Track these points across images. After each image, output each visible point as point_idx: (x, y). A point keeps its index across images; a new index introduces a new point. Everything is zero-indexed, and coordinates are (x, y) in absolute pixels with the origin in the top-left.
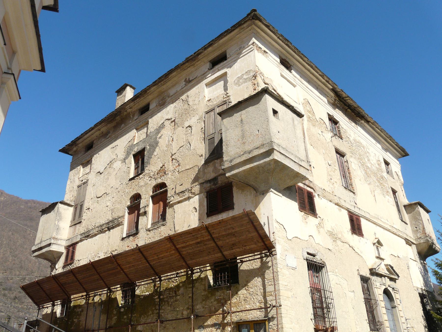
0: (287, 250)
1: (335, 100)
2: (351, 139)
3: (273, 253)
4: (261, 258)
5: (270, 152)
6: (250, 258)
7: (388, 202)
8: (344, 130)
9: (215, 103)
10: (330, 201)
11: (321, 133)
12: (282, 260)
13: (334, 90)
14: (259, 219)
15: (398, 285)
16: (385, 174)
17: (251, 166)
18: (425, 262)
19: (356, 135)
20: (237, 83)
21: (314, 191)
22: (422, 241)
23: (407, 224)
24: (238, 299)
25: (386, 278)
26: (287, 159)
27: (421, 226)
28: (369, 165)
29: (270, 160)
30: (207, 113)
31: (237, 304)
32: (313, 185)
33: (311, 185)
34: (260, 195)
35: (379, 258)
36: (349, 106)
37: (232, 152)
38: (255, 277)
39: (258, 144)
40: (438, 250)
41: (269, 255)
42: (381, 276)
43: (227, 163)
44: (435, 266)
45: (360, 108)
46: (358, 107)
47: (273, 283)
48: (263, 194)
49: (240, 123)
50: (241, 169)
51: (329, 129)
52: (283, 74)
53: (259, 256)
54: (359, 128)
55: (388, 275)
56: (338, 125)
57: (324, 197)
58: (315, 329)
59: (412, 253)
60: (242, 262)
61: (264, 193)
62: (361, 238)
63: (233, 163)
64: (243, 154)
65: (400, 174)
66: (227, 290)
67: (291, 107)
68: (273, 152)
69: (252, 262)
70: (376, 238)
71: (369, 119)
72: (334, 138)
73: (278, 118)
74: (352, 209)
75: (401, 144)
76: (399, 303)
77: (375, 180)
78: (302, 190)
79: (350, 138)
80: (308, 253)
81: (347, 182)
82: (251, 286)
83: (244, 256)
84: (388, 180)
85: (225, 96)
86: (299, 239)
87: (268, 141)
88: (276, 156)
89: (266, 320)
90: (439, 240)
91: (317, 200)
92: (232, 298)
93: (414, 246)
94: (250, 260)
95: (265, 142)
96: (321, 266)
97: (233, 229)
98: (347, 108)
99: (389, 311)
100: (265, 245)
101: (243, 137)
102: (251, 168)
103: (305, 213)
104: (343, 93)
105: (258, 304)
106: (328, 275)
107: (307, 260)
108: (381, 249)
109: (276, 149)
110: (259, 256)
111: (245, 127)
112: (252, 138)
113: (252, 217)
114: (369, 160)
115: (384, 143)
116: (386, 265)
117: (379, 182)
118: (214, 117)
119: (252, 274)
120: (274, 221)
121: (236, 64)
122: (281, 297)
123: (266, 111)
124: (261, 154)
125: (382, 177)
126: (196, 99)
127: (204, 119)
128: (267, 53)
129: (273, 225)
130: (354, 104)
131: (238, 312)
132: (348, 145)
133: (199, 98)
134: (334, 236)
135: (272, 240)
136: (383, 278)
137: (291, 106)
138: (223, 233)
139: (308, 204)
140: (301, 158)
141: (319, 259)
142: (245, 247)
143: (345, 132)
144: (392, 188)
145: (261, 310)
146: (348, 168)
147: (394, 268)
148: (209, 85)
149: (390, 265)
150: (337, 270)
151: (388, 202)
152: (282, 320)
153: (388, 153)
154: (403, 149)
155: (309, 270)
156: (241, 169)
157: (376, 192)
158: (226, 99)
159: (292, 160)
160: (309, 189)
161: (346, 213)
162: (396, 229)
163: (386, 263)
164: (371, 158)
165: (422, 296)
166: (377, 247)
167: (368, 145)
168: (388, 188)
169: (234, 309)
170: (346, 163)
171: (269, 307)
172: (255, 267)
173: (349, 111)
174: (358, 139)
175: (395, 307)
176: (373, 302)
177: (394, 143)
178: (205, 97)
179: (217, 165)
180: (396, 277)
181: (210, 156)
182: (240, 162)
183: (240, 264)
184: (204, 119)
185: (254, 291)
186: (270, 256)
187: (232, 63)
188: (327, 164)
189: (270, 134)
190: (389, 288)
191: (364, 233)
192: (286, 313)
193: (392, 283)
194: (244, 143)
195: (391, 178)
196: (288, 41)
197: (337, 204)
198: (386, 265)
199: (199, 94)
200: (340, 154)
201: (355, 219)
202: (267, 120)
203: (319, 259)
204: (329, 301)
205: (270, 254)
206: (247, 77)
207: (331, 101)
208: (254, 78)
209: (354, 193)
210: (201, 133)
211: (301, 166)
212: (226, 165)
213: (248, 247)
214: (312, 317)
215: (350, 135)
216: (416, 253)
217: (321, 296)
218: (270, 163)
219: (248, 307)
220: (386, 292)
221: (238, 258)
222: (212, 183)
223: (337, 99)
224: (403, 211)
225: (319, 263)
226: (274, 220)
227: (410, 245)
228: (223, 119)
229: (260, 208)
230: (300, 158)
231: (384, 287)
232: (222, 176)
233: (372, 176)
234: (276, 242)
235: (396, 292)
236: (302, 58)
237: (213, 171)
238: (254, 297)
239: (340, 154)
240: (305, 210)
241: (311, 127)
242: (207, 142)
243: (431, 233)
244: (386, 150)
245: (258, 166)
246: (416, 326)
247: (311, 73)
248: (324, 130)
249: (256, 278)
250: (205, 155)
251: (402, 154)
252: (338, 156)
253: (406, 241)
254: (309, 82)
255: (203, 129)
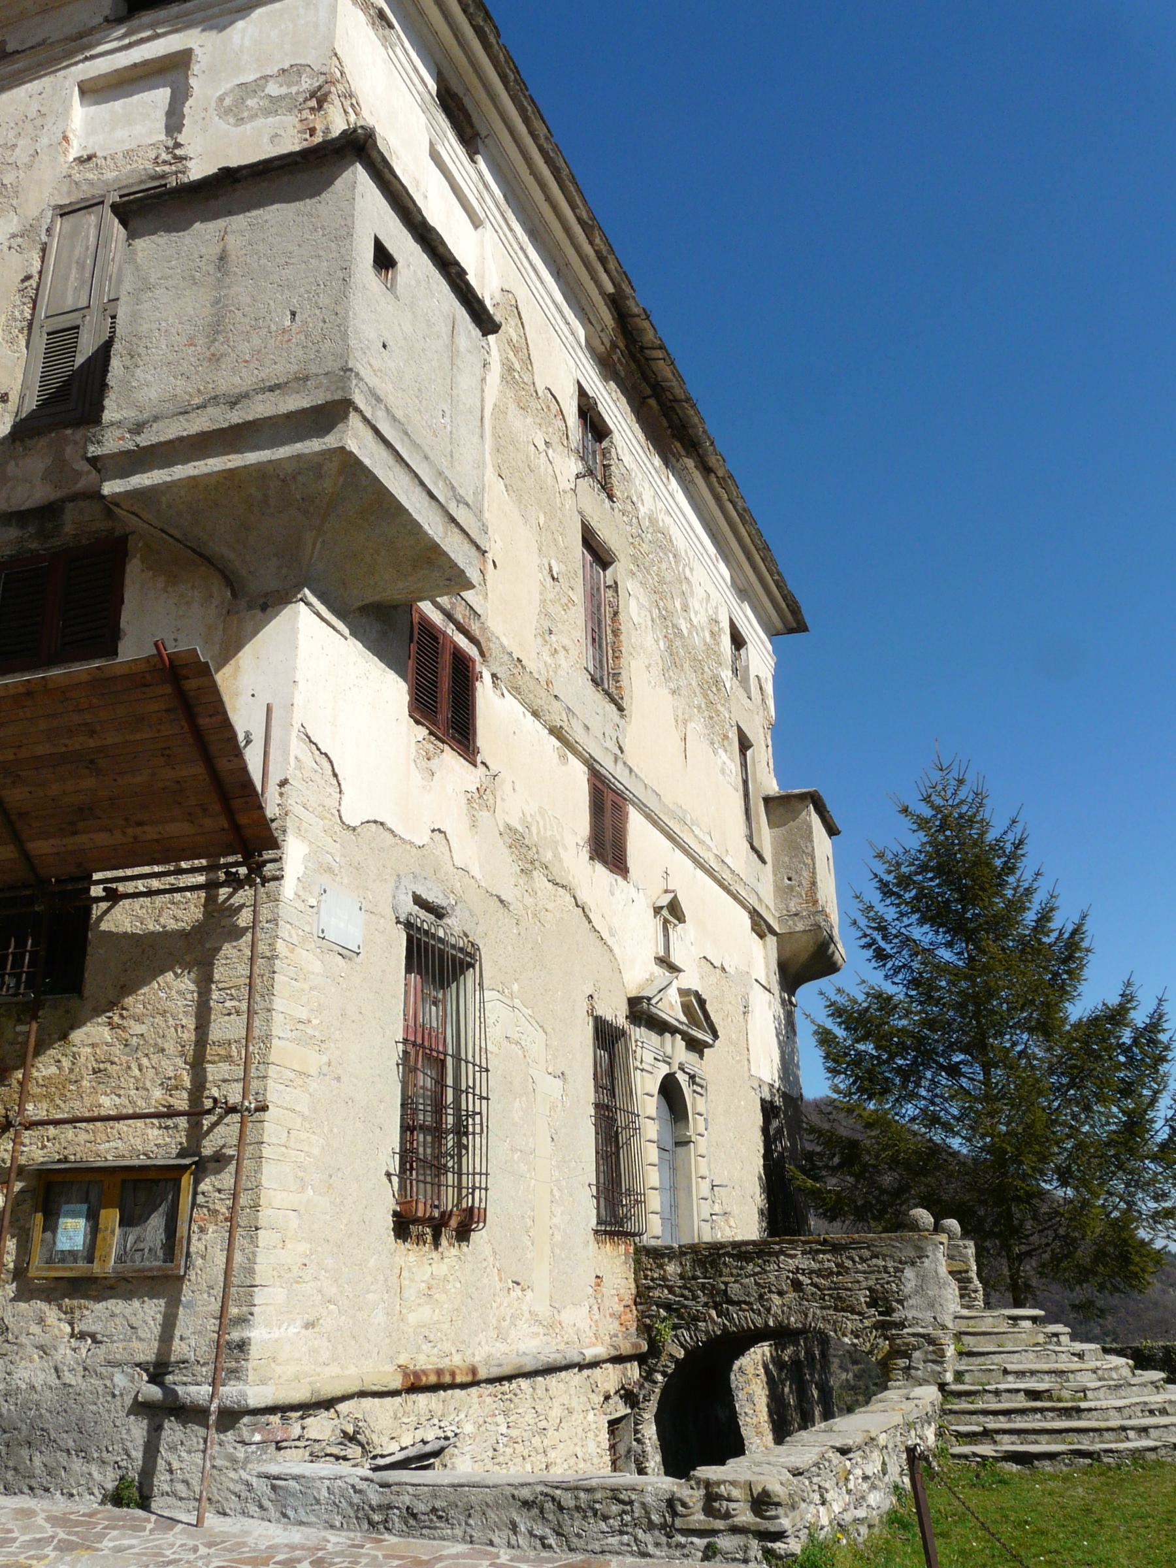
0: (329, 870)
1: (614, 345)
2: (643, 511)
3: (269, 869)
4: (211, 887)
5: (332, 413)
6: (155, 884)
7: (723, 771)
8: (623, 471)
9: (110, 175)
10: (535, 714)
11: (542, 447)
12: (300, 906)
13: (616, 302)
14: (226, 699)
15: (710, 1065)
16: (726, 674)
17: (230, 465)
18: (793, 999)
19: (660, 505)
20: (235, 108)
21: (482, 654)
22: (800, 927)
23: (764, 862)
24: (66, 1063)
25: (678, 1037)
26: (399, 470)
27: (805, 874)
28: (684, 626)
29: (323, 453)
30: (65, 212)
31: (58, 1088)
32: (484, 629)
33: (474, 628)
34: (250, 607)
35: (665, 962)
36: (658, 389)
37: (147, 393)
38: (162, 972)
39: (280, 370)
40: (840, 961)
41: (248, 876)
42: (661, 1027)
43: (118, 433)
44: (826, 1012)
45: (693, 406)
46: (688, 400)
47: (244, 1006)
48: (264, 608)
49: (211, 268)
50: (181, 471)
51: (573, 446)
52: (440, 148)
53: (201, 879)
54: (674, 484)
55: (685, 1028)
56: (604, 444)
57: (516, 691)
58: (395, 1214)
59: (759, 960)
60: (113, 897)
61: (272, 602)
62: (619, 878)
63: (146, 439)
64: (202, 406)
65: (769, 688)
66: (20, 1021)
67: (453, 270)
68: (345, 417)
69: (159, 900)
70: (666, 891)
71: (712, 461)
72: (584, 483)
73: (391, 288)
74: (607, 764)
75: (792, 586)
76: (701, 1128)
77: (694, 684)
78: (436, 639)
79: (639, 505)
80: (419, 901)
81: (601, 661)
82: (139, 1009)
83: (129, 872)
84: (732, 697)
85: (165, 156)
86: (388, 835)
87: (331, 365)
88: (354, 438)
89: (186, 1168)
90: (853, 929)
91: (484, 692)
92: (37, 1053)
93: (771, 940)
94: (150, 893)
95: (313, 369)
96: (461, 962)
97: (92, 733)
98: (648, 392)
99: (666, 1155)
100: (236, 827)
101: (216, 329)
102: (231, 473)
103: (431, 733)
104: (646, 324)
105: (158, 1093)
106: (482, 1002)
107: (408, 925)
108: (678, 933)
109: (362, 406)
110: (201, 879)
111: (235, 289)
112: (256, 342)
113: (191, 685)
114: (685, 609)
115: (741, 567)
116: (683, 992)
117: (705, 696)
118: (92, 240)
119: (151, 955)
120: (294, 733)
121: (240, 24)
122: (272, 1071)
123: (345, 235)
124: (289, 416)
125: (717, 681)
126: (21, 142)
127: (44, 238)
128: (391, 26)
129: (286, 752)
130: (675, 384)
131: (56, 1123)
132: (628, 528)
133: (35, 140)
134: (524, 849)
135: (271, 811)
136: (668, 1035)
137: (457, 264)
138: (40, 750)
139: (445, 700)
140: (461, 491)
141: (457, 930)
142: (138, 830)
143: (627, 478)
144: (739, 729)
145: (170, 1122)
146: (616, 614)
147: (708, 1006)
148: (92, 91)
149: (697, 995)
150: (516, 987)
151: (723, 771)
152: (258, 1170)
153: (746, 606)
154: (796, 603)
155: (409, 970)
156: (181, 471)
157: (691, 725)
158: (167, 168)
159: (422, 484)
160: (462, 641)
161: (580, 772)
162: (733, 872)
163: (685, 986)
164: (694, 603)
165: (768, 1110)
166: (666, 921)
167: (691, 554)
168: (727, 727)
169: (33, 1110)
170: (610, 593)
171: (209, 1112)
172: (172, 925)
173: (651, 408)
174: (664, 520)
175: (687, 1143)
176: (621, 1119)
177: (772, 575)
178: (66, 138)
179: (69, 450)
180: (708, 1039)
181: (44, 405)
182: (181, 439)
183: (104, 905)
184: (44, 238)
185: (151, 1037)
186: (249, 881)
187: (227, 18)
188: (546, 572)
189: (345, 336)
190: (682, 1078)
191: (632, 862)
192: (283, 1140)
193: (692, 1057)
194: (216, 359)
195: (741, 694)
196: (487, 14)
197: (556, 732)
198: (683, 992)
199: (38, 122)
200: (598, 553)
201: (608, 805)
202: (340, 274)
203: (457, 930)
204: (469, 1103)
205: (251, 871)
206: (284, 90)
207: (597, 343)
208: (313, 103)
209: (621, 709)
210: (17, 299)
211: (453, 520)
212: (112, 442)
213: (151, 832)
214: (394, 1165)
215: (640, 496)
216: (774, 966)
217: (440, 1082)
218: (320, 466)
219: (108, 1104)
220: (670, 1091)
221: (97, 876)
222: (32, 530)
223: (621, 345)
224: (758, 815)
225: (453, 947)
226: (297, 726)
227: (762, 936)
228: (132, 235)
229: (237, 668)
230: (453, 488)
231: (664, 1070)
232: (81, 504)
233: (686, 666)
234: (289, 823)
235: (699, 1089)
236: (526, 121)
237: (47, 476)
238: (145, 1061)
239: (598, 553)
240: (434, 724)
241: (512, 407)
242: (41, 342)
243: (829, 904)
244: (743, 593)
245: (259, 472)
246: (735, 1210)
247: (549, 199)
248: (555, 440)
249: (170, 975)
250: (22, 398)
251: (788, 622)
252: (589, 558)
253: (751, 918)
254: (534, 234)
255: (33, 283)
